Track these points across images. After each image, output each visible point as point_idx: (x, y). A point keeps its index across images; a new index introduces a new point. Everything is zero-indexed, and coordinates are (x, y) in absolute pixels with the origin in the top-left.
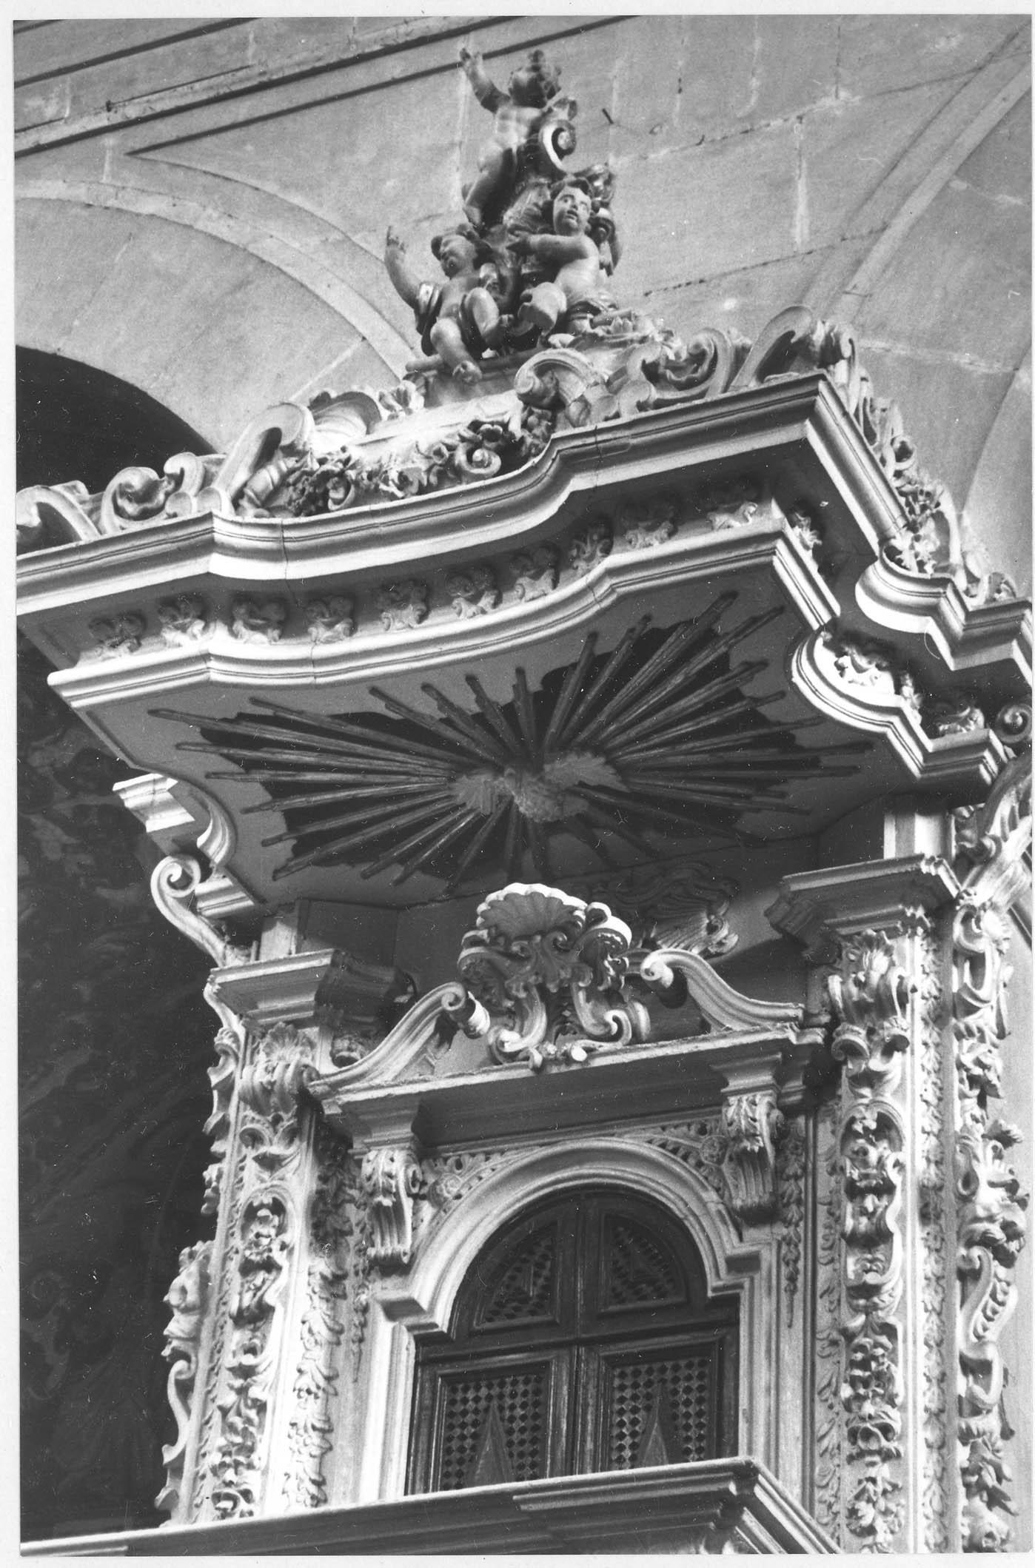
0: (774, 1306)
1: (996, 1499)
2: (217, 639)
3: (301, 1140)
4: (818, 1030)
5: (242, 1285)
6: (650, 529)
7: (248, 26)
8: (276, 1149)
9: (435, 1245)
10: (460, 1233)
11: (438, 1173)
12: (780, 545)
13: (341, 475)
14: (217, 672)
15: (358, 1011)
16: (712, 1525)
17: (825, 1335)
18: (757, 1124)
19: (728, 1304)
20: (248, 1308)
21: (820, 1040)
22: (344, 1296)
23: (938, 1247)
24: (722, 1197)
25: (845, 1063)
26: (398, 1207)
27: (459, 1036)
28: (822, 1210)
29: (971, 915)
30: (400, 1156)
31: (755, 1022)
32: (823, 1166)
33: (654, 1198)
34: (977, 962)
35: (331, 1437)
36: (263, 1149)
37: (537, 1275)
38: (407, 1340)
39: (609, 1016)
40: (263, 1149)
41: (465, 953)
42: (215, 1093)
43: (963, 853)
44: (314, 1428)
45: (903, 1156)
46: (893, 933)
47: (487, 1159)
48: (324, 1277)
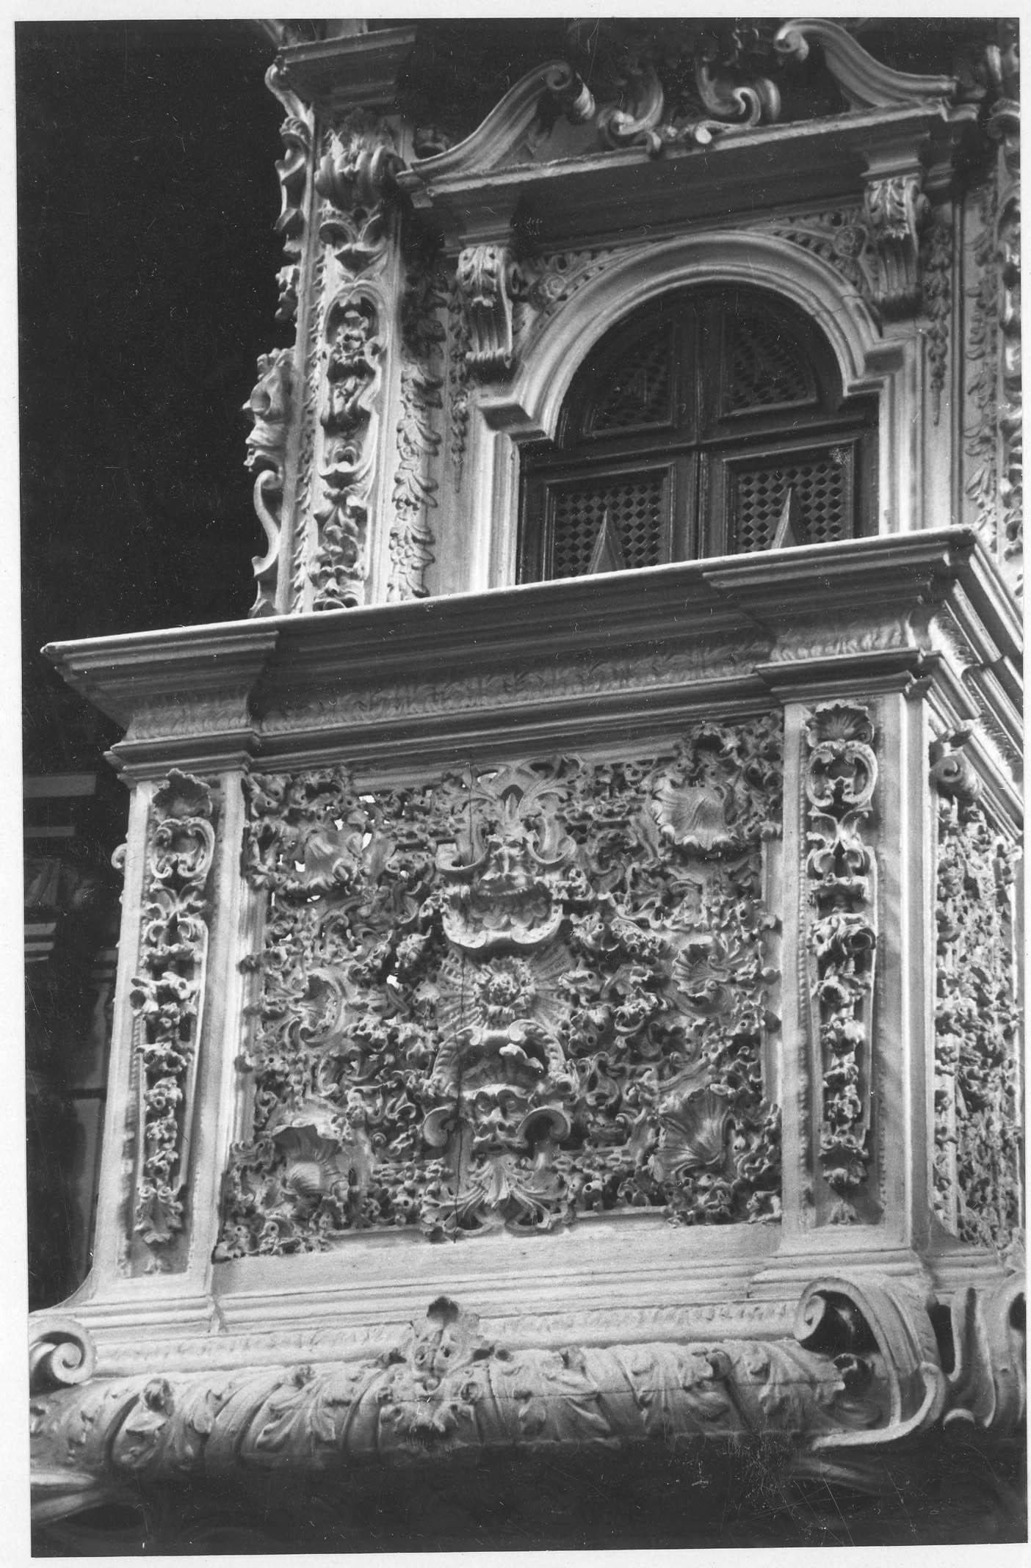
0: (919, 403)
3: (388, 238)
4: (973, 106)
5: (332, 391)
9: (540, 348)
10: (566, 337)
11: (539, 273)
16: (920, 598)
17: (974, 432)
18: (904, 210)
19: (866, 405)
20: (341, 414)
21: (974, 116)
22: (440, 405)
24: (859, 290)
25: (1002, 141)
26: (499, 306)
28: (970, 303)
30: (500, 253)
32: (970, 256)
33: (781, 295)
35: (434, 549)
37: (651, 380)
38: (510, 448)
39: (738, 93)
42: (284, 191)
44: (415, 539)
47: (593, 257)
48: (417, 384)
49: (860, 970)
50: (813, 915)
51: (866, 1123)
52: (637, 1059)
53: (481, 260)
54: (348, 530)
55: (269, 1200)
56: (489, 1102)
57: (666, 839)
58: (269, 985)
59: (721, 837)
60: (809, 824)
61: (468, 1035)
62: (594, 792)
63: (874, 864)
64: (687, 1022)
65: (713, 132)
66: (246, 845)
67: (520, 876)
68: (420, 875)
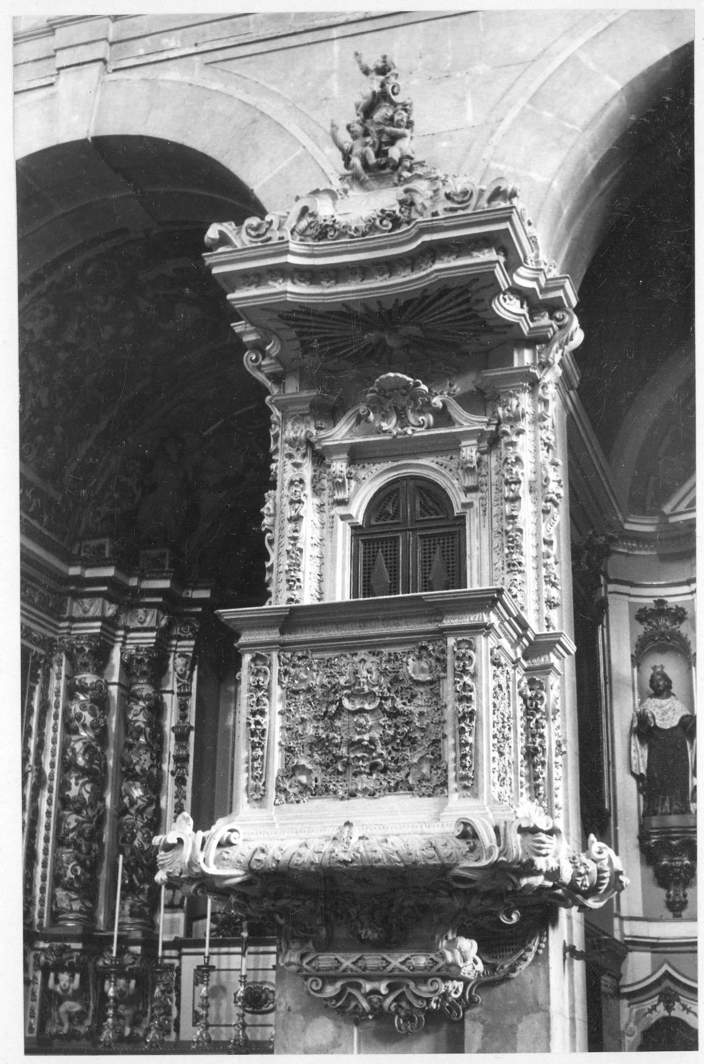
1: (554, 585)
2: (289, 287)
6: (449, 256)
7: (251, 17)
8: (299, 460)
12: (497, 265)
13: (332, 226)
14: (289, 298)
15: (328, 413)
19: (462, 518)
23: (535, 501)
26: (344, 482)
27: (363, 422)
28: (494, 488)
29: (545, 386)
30: (344, 465)
31: (472, 423)
32: (493, 472)
34: (546, 403)
35: (324, 560)
36: (294, 461)
38: (348, 528)
39: (420, 419)
40: (294, 461)
41: (368, 395)
43: (541, 363)
45: (524, 471)
46: (519, 392)
49: (470, 722)
50: (457, 704)
51: (473, 768)
52: (403, 745)
53: (339, 466)
54: (297, 555)
55: (290, 786)
56: (358, 759)
57: (411, 678)
58: (288, 719)
59: (429, 678)
60: (455, 675)
61: (351, 738)
62: (389, 661)
63: (475, 689)
64: (417, 735)
65: (413, 430)
66: (280, 675)
67: (366, 688)
68: (334, 687)
